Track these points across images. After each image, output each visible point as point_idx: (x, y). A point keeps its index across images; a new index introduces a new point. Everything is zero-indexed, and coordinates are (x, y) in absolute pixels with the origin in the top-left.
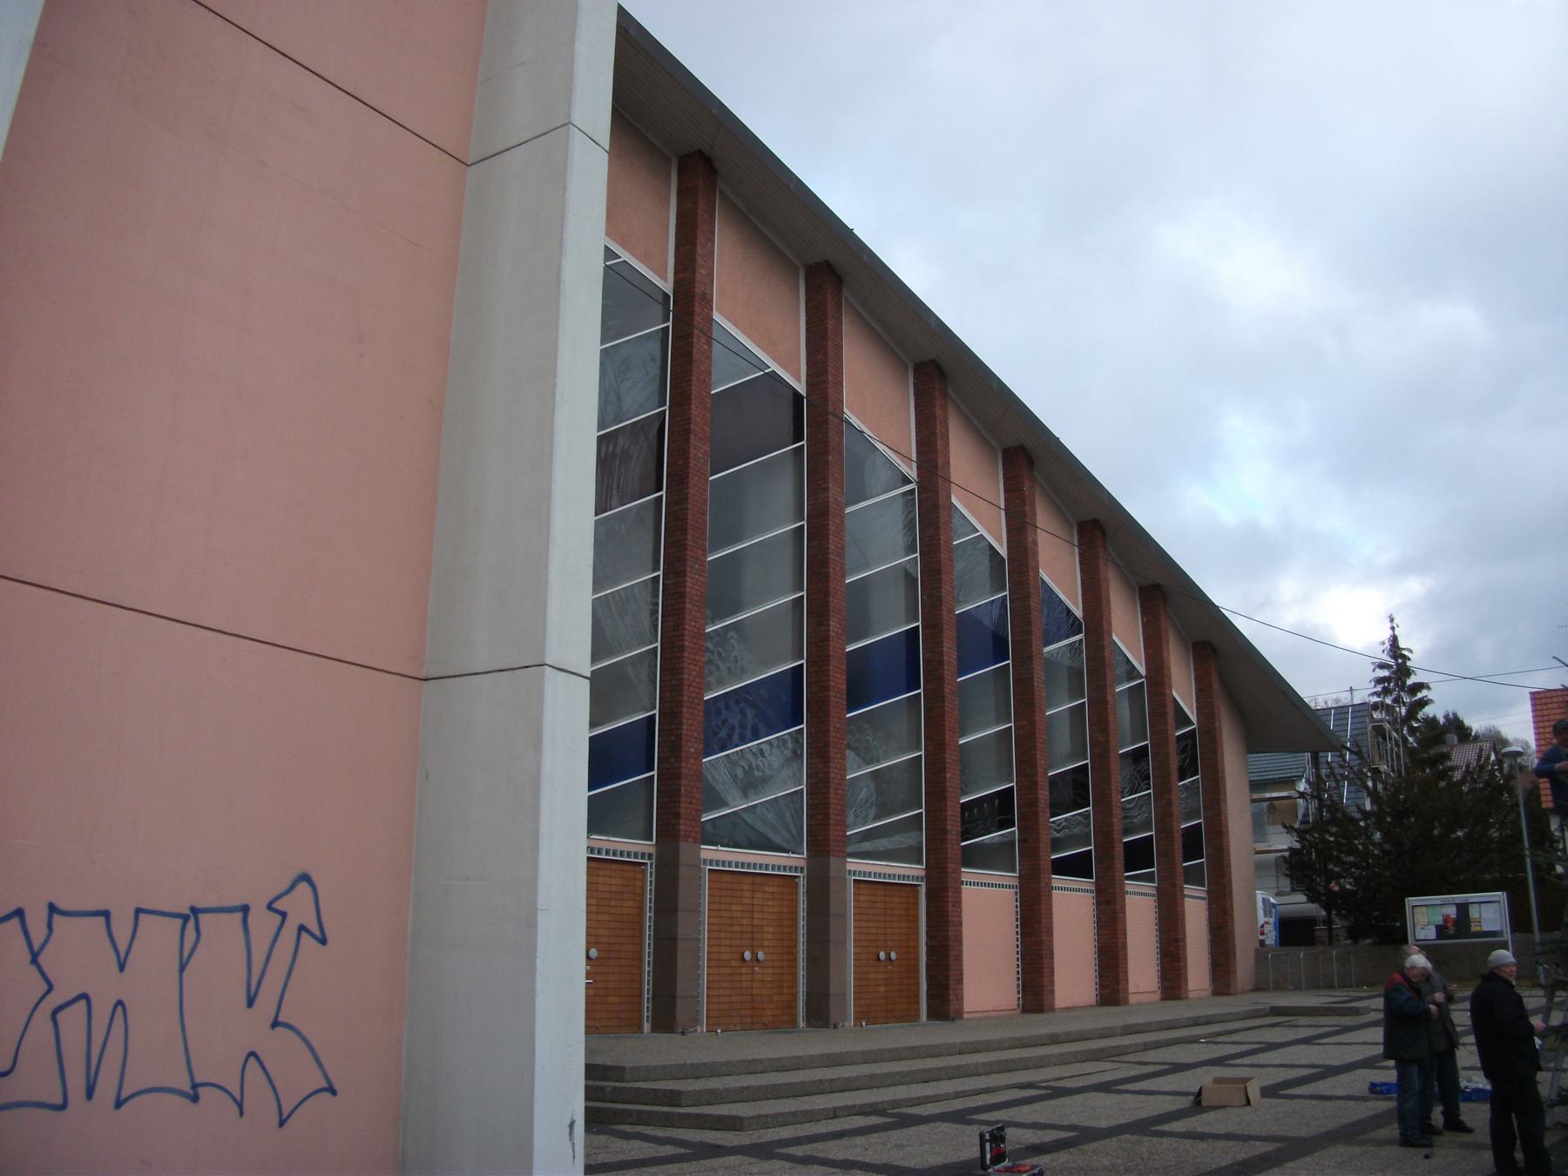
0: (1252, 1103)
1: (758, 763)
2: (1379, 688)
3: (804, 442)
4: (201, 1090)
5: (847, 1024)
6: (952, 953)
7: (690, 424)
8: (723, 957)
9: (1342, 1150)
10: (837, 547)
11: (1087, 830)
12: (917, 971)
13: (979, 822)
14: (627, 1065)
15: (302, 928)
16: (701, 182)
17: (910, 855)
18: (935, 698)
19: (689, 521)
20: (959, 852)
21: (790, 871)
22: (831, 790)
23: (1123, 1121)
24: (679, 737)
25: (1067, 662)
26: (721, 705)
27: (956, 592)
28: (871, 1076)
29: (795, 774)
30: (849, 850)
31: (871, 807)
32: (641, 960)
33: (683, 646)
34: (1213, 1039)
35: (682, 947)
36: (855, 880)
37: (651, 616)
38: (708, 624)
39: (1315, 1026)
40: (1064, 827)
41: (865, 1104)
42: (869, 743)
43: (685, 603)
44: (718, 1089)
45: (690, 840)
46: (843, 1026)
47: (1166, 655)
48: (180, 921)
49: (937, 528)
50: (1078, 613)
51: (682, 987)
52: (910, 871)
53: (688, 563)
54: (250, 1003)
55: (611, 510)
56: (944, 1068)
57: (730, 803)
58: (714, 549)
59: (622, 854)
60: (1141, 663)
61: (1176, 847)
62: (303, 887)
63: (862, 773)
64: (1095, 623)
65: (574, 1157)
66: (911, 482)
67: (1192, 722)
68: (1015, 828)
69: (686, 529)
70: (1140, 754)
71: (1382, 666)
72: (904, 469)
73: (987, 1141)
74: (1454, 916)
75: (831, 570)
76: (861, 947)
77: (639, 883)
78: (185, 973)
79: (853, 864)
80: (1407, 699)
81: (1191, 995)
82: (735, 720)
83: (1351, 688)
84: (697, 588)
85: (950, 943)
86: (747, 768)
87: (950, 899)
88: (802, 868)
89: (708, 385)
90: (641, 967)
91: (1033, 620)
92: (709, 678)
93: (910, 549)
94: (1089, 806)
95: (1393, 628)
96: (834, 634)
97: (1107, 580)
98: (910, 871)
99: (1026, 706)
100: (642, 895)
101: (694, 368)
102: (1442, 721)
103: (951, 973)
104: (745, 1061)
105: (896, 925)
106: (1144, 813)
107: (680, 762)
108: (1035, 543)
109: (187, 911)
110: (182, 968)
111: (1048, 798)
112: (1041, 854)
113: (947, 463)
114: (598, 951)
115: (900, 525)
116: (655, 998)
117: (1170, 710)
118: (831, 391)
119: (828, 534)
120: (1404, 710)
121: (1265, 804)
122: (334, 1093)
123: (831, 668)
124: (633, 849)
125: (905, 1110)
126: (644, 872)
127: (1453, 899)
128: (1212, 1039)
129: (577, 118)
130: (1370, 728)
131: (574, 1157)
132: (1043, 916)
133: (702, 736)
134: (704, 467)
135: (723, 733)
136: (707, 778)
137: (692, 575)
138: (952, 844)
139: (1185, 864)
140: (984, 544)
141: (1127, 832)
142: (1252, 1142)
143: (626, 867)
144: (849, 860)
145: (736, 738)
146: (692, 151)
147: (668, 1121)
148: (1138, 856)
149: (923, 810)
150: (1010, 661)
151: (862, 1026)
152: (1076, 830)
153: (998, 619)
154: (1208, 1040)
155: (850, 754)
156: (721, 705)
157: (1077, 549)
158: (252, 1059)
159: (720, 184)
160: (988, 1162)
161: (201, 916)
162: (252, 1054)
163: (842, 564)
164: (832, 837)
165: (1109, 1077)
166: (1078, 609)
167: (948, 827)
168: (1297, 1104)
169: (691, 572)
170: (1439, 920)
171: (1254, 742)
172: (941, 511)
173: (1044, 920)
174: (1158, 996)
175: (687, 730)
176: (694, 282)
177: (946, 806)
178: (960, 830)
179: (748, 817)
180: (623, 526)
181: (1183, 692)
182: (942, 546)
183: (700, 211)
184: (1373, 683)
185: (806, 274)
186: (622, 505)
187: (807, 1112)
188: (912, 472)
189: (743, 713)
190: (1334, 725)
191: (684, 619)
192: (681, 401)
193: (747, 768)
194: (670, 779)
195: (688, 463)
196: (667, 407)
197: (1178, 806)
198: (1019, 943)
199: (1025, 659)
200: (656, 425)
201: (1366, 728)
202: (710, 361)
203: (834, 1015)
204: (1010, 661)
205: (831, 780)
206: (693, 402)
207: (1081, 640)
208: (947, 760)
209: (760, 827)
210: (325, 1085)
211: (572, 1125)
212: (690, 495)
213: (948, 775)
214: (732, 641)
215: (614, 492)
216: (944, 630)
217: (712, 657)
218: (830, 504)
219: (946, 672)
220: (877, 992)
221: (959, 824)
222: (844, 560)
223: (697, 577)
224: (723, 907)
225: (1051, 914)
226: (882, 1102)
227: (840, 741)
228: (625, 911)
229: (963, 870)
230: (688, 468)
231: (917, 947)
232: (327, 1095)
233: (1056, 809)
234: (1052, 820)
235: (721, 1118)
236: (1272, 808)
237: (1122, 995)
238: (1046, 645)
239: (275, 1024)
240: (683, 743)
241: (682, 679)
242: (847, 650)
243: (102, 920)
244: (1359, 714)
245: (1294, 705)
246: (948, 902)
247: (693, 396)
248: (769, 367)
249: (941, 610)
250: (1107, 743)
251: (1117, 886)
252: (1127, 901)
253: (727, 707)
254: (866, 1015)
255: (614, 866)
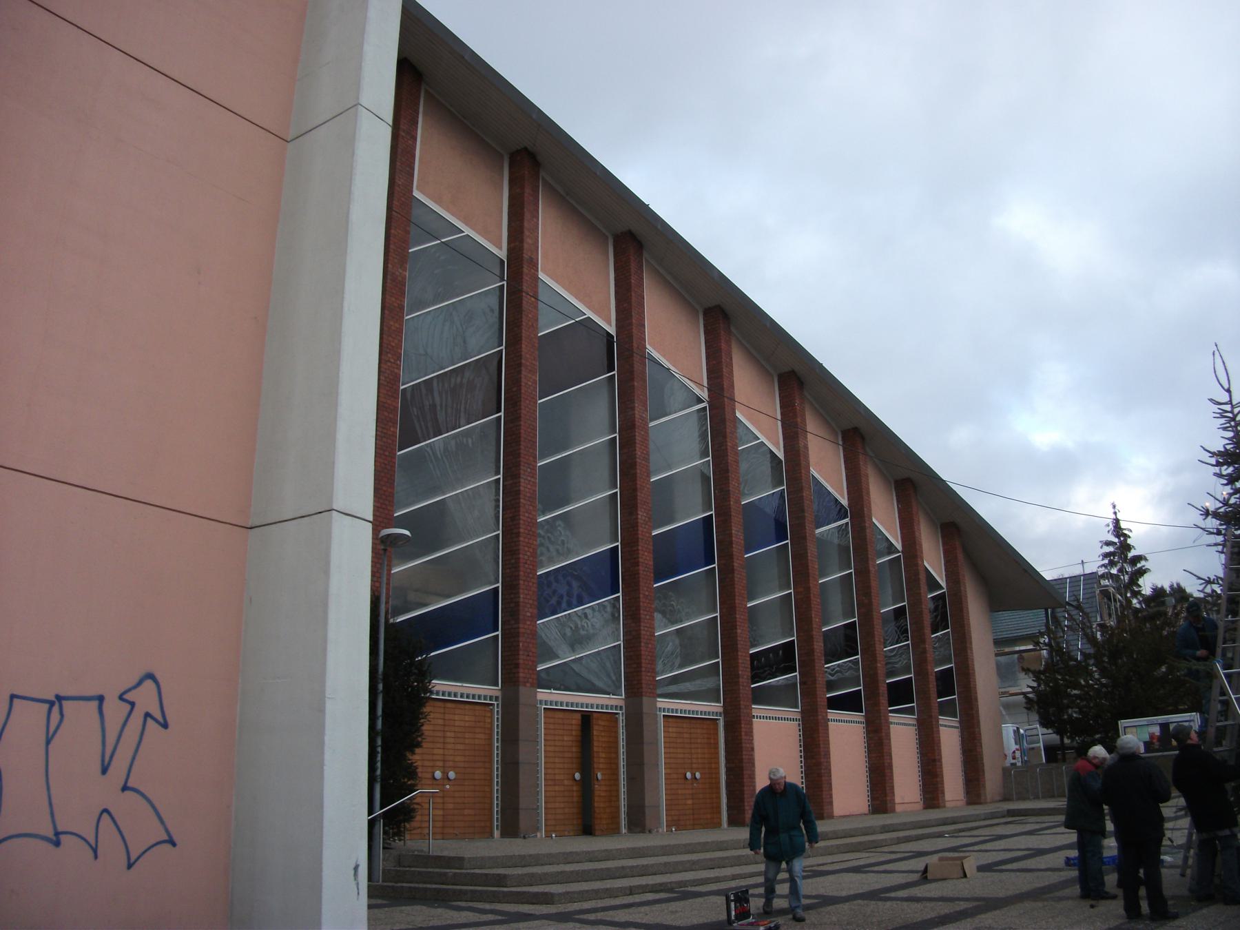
0: (968, 876)
1: (583, 624)
2: (1106, 561)
3: (615, 372)
4: (62, 837)
5: (660, 830)
6: (746, 772)
7: (521, 359)
8: (557, 777)
9: (1028, 905)
10: (642, 453)
11: (856, 674)
12: (718, 788)
13: (766, 669)
14: (466, 856)
15: (147, 715)
16: (526, 172)
17: (711, 695)
18: (727, 571)
19: (522, 435)
20: (750, 692)
21: (611, 709)
22: (642, 644)
23: (861, 891)
24: (517, 604)
25: (836, 541)
26: (552, 578)
27: (742, 486)
28: (665, 864)
29: (613, 632)
30: (659, 691)
31: (676, 657)
32: (491, 780)
33: (519, 532)
34: (956, 835)
35: (523, 769)
36: (544, 708)
37: (495, 509)
38: (539, 515)
39: (1041, 823)
40: (837, 672)
41: (656, 884)
42: (674, 607)
43: (519, 498)
44: (537, 873)
45: (528, 685)
46: (658, 831)
47: (917, 534)
48: (46, 706)
49: (725, 437)
50: (844, 502)
51: (524, 802)
52: (711, 708)
53: (522, 467)
54: (104, 770)
55: (459, 428)
56: (727, 858)
57: (560, 656)
58: (543, 457)
59: (474, 697)
60: (897, 541)
61: (931, 686)
62: (149, 684)
63: (668, 630)
64: (858, 509)
65: (358, 893)
66: (704, 402)
67: (941, 586)
68: (797, 673)
69: (520, 441)
70: (899, 613)
71: (1108, 543)
72: (697, 391)
73: (732, 901)
74: (1159, 734)
75: (638, 471)
76: (671, 768)
77: (488, 720)
78: (50, 746)
79: (662, 703)
80: (1129, 569)
81: (948, 804)
82: (563, 590)
83: (1082, 561)
84: (529, 487)
85: (744, 765)
86: (574, 628)
87: (743, 730)
88: (621, 707)
89: (535, 328)
90: (491, 786)
91: (806, 508)
92: (541, 558)
93: (704, 454)
94: (858, 654)
95: (1115, 513)
96: (642, 522)
97: (867, 476)
98: (711, 708)
99: (803, 576)
100: (491, 729)
101: (524, 316)
102: (1168, 589)
103: (745, 788)
104: (564, 853)
105: (699, 751)
106: (904, 659)
107: (519, 623)
108: (806, 447)
109: (54, 699)
110: (48, 742)
111: (822, 648)
112: (818, 693)
113: (732, 386)
114: (456, 773)
115: (696, 434)
116: (503, 811)
117: (922, 576)
118: (635, 331)
119: (635, 443)
120: (1127, 577)
121: (1016, 656)
122: (174, 844)
123: (640, 548)
124: (482, 693)
125: (690, 889)
126: (492, 711)
127: (1157, 720)
128: (954, 835)
129: (364, 100)
130: (1098, 592)
131: (358, 893)
132: (821, 742)
133: (536, 603)
134: (534, 393)
135: (554, 601)
136: (541, 637)
137: (525, 477)
138: (743, 686)
139: (939, 700)
140: (764, 449)
141: (891, 674)
142: (957, 902)
143: (477, 707)
144: (659, 699)
145: (564, 605)
146: (519, 148)
147: (495, 898)
148: (900, 694)
149: (720, 660)
150: (788, 541)
151: (672, 831)
152: (847, 674)
153: (778, 507)
154: (951, 835)
155: (657, 616)
156: (552, 578)
157: (841, 448)
158: (105, 815)
159: (542, 174)
160: (733, 918)
161: (64, 702)
162: (106, 811)
163: (647, 466)
164: (643, 682)
165: (861, 863)
166: (844, 498)
167: (740, 673)
168: (1004, 876)
169: (524, 474)
170: (1147, 737)
171: (996, 602)
172: (727, 423)
173: (822, 746)
174: (920, 806)
175: (523, 598)
176: (523, 250)
177: (738, 655)
178: (749, 674)
179: (575, 667)
180: (470, 441)
181: (933, 563)
182: (729, 451)
183: (526, 195)
184: (1101, 557)
185: (614, 242)
186: (468, 424)
187: (607, 889)
188: (704, 394)
189: (569, 584)
190: (1083, 599)
191: (519, 511)
192: (514, 342)
193: (574, 628)
194: (511, 637)
195: (520, 389)
196: (503, 347)
197: (931, 655)
198: (803, 764)
199: (800, 539)
200: (495, 363)
201: (1095, 592)
202: (537, 310)
203: (649, 822)
204: (788, 541)
205: (642, 636)
206: (523, 342)
207: (847, 523)
208: (738, 619)
209: (585, 673)
210: (166, 837)
211: (356, 868)
212: (522, 415)
213: (739, 631)
214: (559, 528)
215: (462, 414)
216: (732, 517)
217: (543, 541)
218: (637, 419)
219: (734, 550)
220: (686, 804)
221: (749, 670)
222: (649, 463)
223: (529, 478)
224: (557, 738)
225: (828, 741)
226: (670, 883)
227: (649, 605)
228: (477, 742)
229: (753, 706)
230: (520, 393)
231: (718, 768)
232: (168, 847)
233: (831, 656)
234: (826, 666)
235: (536, 895)
236: (1021, 659)
237: (889, 805)
238: (817, 528)
239: (125, 788)
240: (521, 608)
241: (519, 558)
242: (653, 534)
243: (16, 701)
244: (1089, 581)
245: (1026, 571)
246: (741, 732)
247: (523, 338)
248: (585, 314)
249: (730, 501)
250: (870, 603)
251: (882, 718)
252: (892, 730)
253: (557, 581)
254: (677, 823)
255: (467, 707)
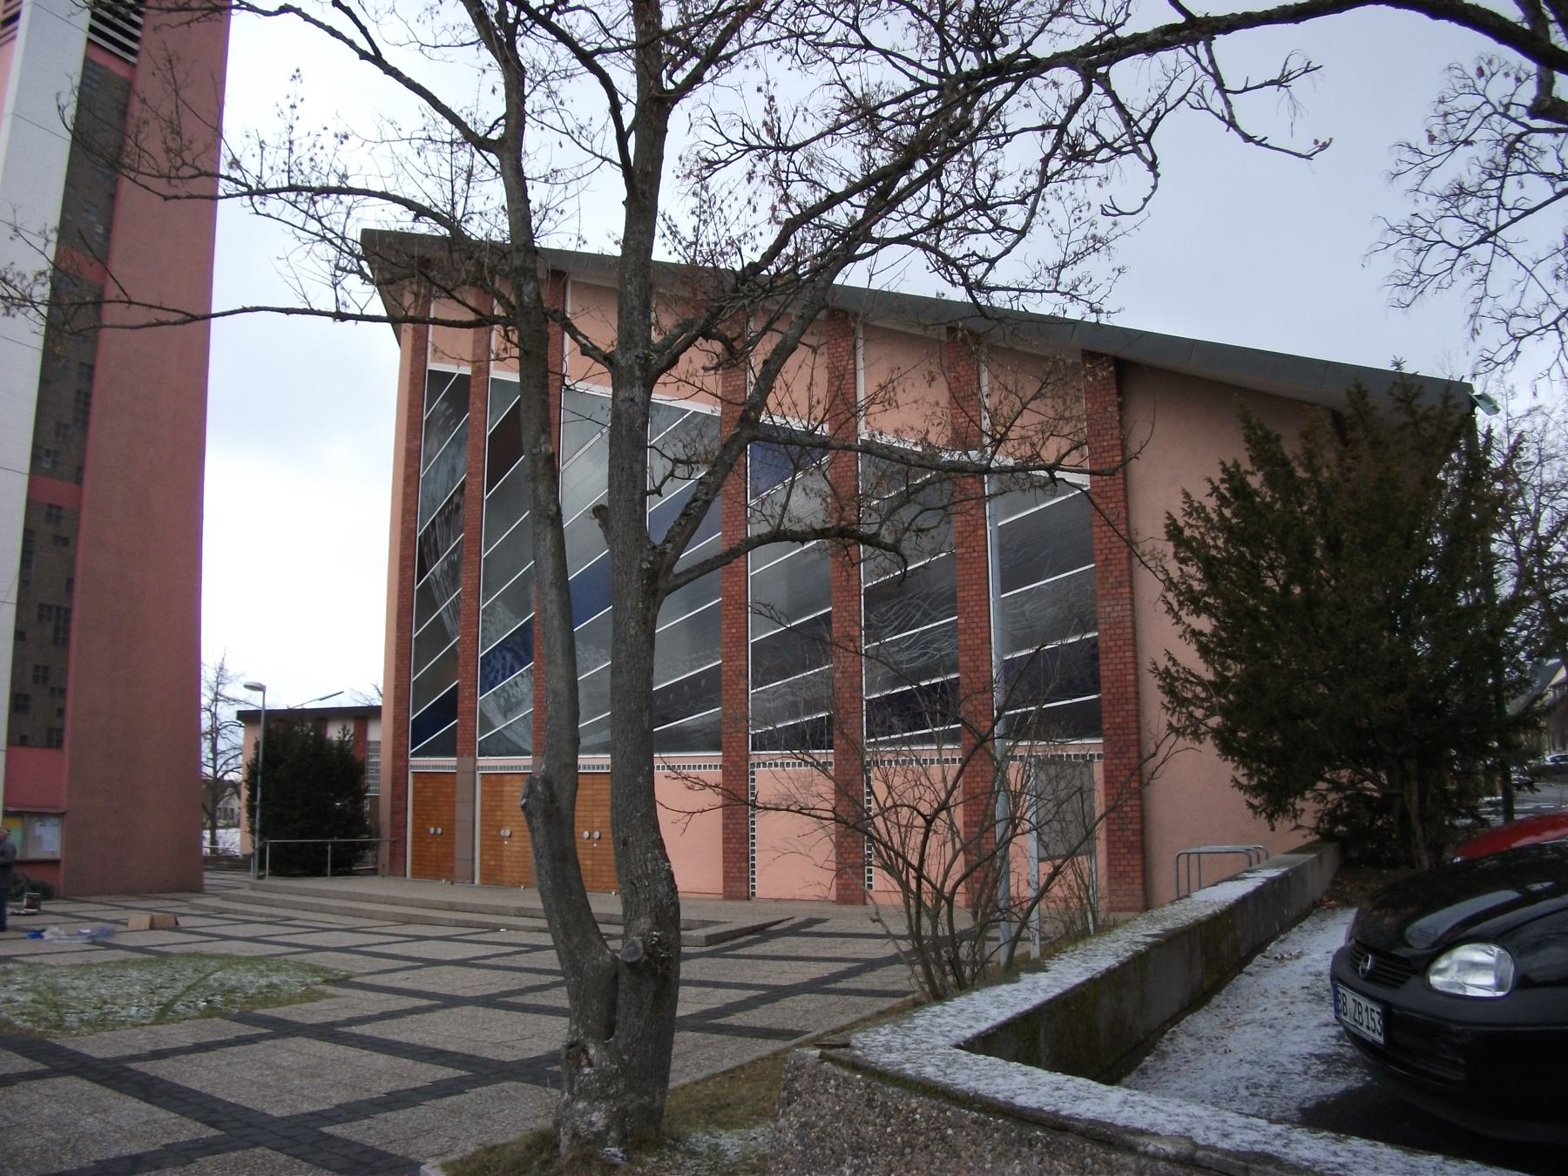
11: (499, 603)
145: (500, 678)
156: (491, 657)
189: (504, 658)
